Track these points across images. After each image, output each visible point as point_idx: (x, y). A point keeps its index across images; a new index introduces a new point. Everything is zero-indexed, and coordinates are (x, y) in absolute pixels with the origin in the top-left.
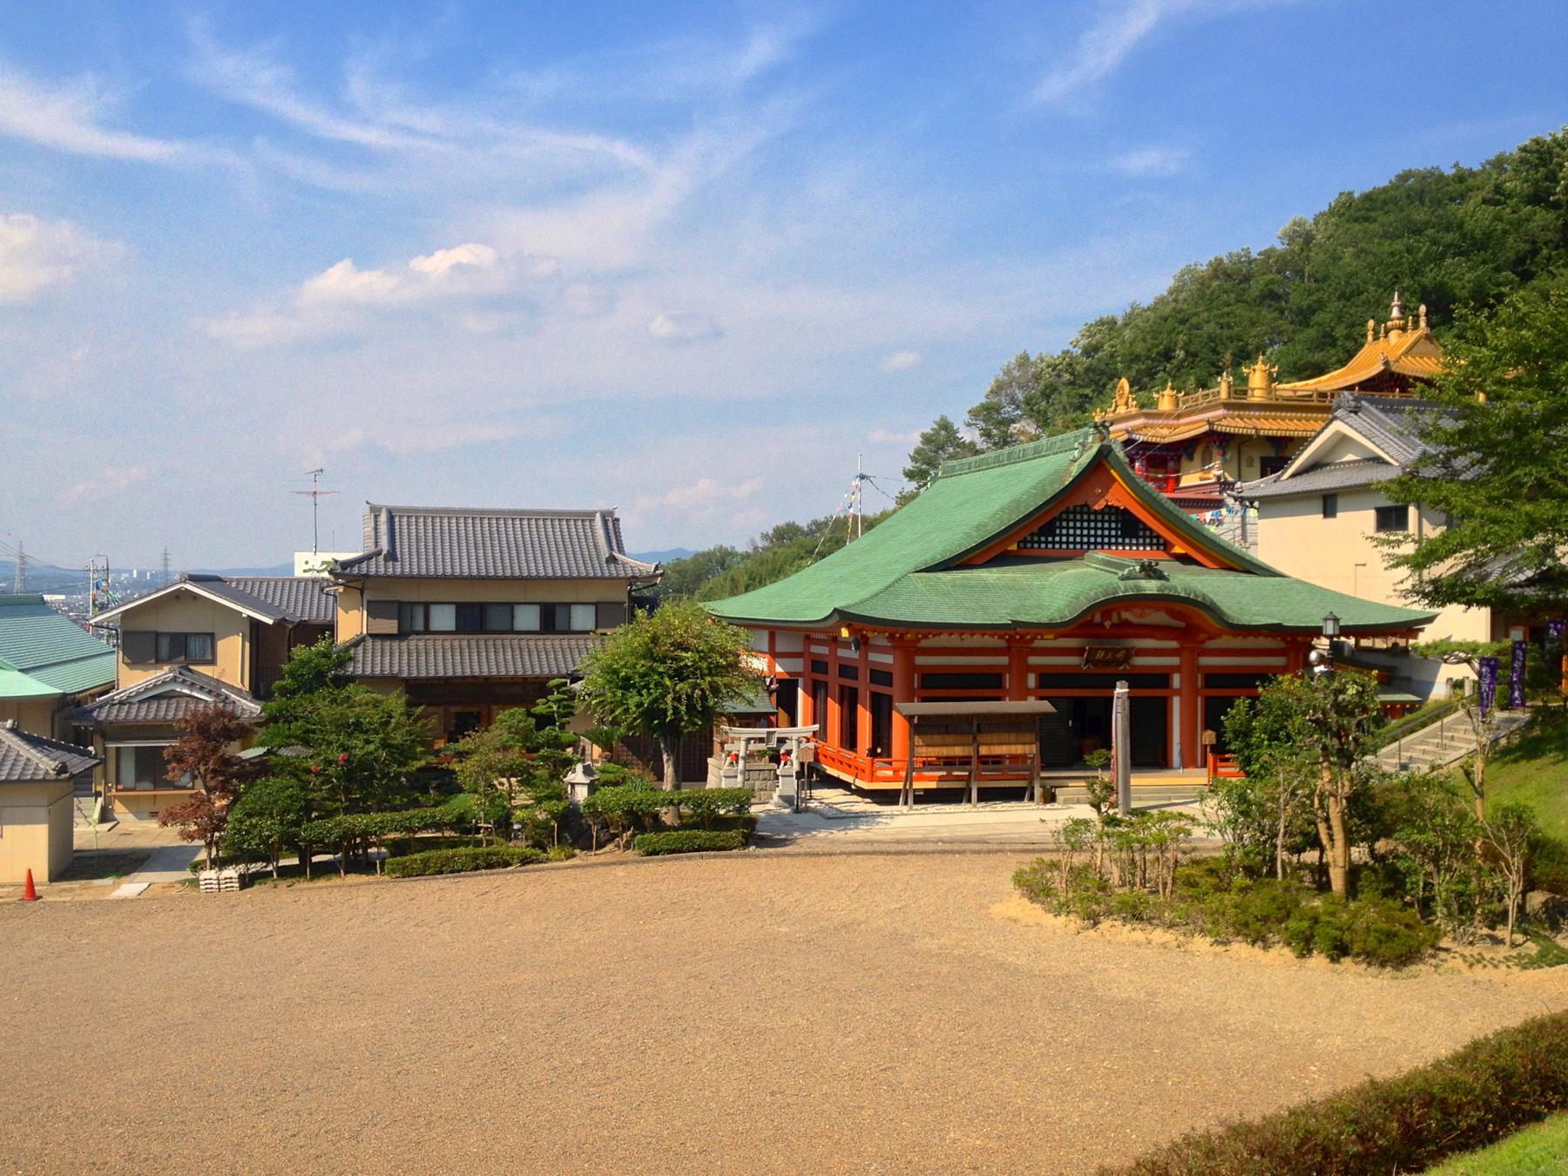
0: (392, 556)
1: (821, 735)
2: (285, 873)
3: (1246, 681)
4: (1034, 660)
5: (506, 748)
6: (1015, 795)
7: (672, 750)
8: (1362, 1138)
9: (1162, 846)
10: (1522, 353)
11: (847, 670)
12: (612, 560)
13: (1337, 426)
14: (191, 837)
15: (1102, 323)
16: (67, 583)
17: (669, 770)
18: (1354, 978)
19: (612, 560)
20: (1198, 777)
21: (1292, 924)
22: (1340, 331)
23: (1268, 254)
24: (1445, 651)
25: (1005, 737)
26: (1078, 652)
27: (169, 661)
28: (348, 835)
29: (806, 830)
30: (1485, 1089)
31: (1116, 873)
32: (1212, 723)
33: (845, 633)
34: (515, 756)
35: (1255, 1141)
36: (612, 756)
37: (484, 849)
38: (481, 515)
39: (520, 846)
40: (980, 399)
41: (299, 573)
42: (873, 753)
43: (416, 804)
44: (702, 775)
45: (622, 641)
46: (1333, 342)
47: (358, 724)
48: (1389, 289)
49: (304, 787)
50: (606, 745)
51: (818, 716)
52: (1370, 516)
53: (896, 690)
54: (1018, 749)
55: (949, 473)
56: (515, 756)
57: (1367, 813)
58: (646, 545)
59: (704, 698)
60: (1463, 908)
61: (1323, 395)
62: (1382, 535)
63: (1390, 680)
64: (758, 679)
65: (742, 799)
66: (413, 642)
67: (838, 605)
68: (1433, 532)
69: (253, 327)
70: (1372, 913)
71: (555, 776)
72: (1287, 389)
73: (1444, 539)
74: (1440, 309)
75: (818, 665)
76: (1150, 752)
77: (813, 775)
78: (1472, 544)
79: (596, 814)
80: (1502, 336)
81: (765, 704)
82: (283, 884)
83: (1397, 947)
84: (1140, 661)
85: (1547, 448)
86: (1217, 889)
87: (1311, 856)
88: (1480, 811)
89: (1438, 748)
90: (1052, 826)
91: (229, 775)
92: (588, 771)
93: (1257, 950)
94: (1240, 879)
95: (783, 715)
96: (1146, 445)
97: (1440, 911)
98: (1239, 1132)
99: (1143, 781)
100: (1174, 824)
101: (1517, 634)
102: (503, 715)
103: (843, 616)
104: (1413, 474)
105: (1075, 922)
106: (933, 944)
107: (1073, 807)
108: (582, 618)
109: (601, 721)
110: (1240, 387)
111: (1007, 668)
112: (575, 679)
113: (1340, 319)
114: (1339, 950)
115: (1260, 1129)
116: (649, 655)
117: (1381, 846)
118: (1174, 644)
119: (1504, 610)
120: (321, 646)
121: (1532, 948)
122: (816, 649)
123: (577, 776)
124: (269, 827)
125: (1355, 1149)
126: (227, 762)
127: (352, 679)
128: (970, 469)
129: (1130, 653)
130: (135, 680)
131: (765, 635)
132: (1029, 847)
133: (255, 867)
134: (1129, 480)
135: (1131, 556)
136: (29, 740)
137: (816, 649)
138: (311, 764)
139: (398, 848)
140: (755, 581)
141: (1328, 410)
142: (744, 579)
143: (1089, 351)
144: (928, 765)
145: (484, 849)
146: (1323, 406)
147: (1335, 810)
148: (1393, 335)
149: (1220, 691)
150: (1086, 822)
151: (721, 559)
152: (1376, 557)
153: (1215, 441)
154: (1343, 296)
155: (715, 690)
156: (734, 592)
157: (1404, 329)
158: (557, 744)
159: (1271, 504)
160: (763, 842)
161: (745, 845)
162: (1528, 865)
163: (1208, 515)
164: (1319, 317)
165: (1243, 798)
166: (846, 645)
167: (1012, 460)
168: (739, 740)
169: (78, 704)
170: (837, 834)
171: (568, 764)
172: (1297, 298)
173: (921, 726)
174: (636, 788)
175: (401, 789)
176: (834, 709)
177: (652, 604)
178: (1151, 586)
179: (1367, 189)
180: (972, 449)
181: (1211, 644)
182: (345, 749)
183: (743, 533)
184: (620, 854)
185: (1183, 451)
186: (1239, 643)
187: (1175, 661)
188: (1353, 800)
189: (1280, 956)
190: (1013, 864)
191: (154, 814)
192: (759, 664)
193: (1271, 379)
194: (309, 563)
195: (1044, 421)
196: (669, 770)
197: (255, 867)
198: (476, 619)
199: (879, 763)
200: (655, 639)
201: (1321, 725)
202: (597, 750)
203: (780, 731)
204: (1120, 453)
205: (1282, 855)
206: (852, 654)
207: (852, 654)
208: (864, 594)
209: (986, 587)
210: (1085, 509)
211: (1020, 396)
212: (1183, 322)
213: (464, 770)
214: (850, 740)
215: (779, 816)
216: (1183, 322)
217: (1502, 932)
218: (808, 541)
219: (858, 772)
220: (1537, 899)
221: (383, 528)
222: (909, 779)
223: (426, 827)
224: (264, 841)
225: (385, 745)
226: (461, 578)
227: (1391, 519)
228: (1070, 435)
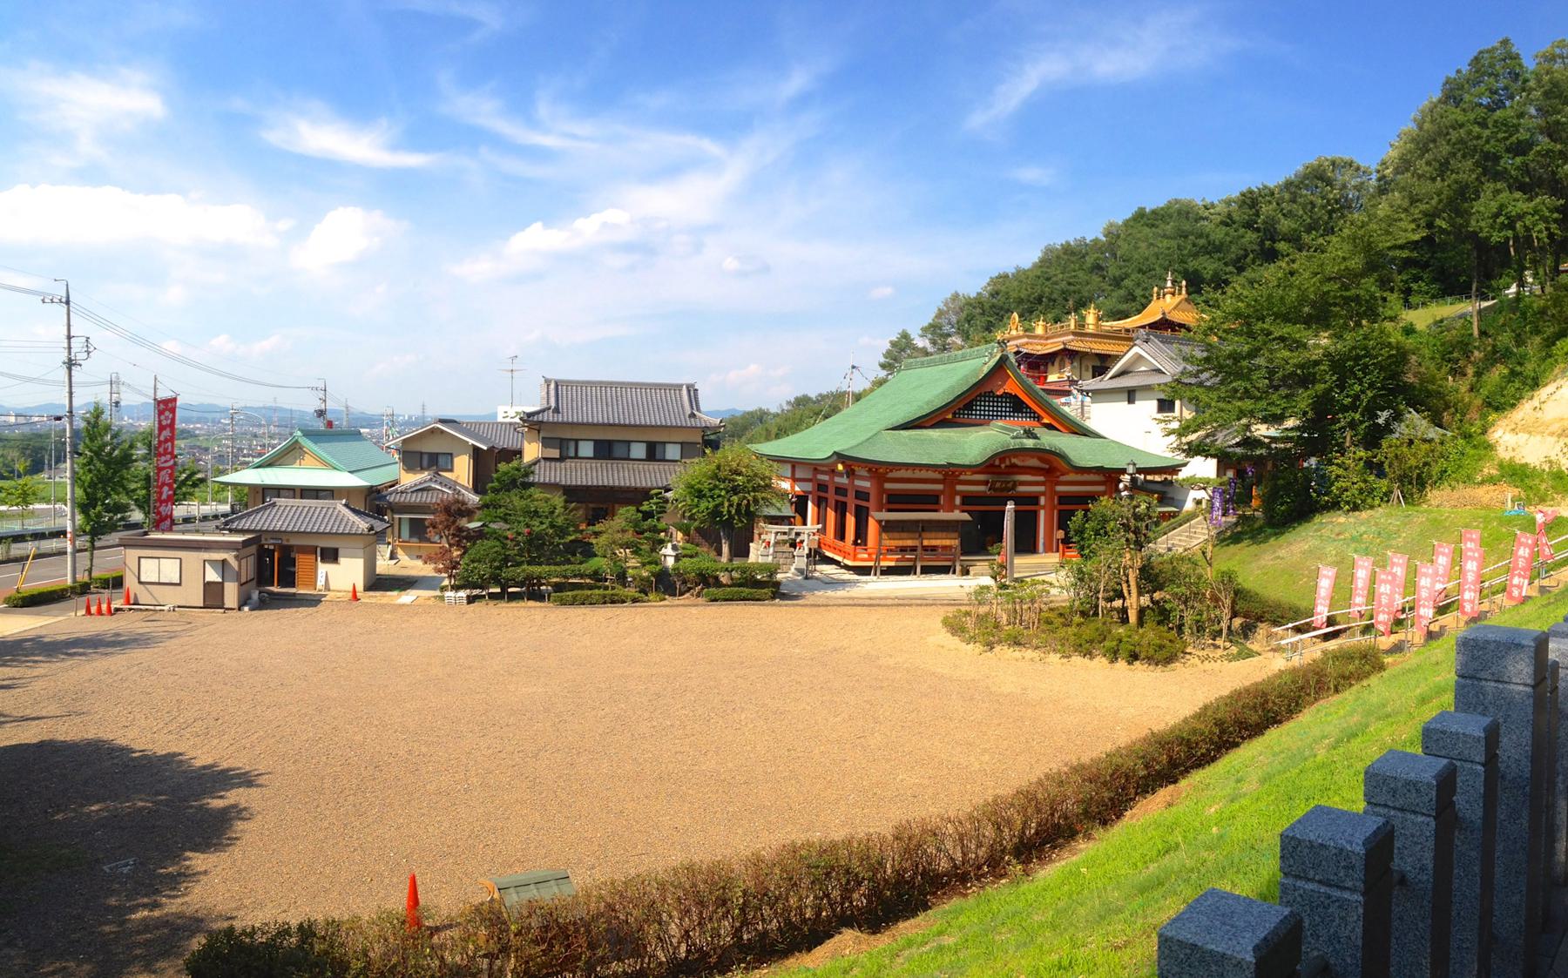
0: (557, 410)
1: (823, 531)
2: (493, 596)
3: (1083, 500)
4: (959, 488)
5: (624, 531)
6: (944, 570)
7: (729, 538)
8: (1147, 767)
9: (1033, 601)
10: (1238, 315)
11: (840, 490)
12: (693, 415)
13: (1136, 350)
14: (440, 571)
15: (1000, 277)
16: (372, 422)
17: (725, 549)
18: (1142, 674)
19: (693, 415)
20: (1054, 558)
21: (1107, 643)
22: (1139, 292)
23: (1096, 241)
24: (1193, 483)
25: (940, 535)
26: (986, 483)
27: (427, 469)
28: (529, 578)
29: (812, 590)
30: (1211, 732)
31: (1005, 617)
32: (1062, 525)
33: (840, 467)
34: (629, 536)
35: (1087, 775)
36: (689, 538)
37: (609, 592)
38: (611, 385)
39: (631, 591)
40: (928, 319)
41: (500, 419)
42: (855, 543)
43: (569, 562)
44: (747, 554)
45: (698, 469)
46: (1134, 299)
47: (536, 512)
48: (1166, 270)
49: (504, 546)
50: (686, 532)
51: (821, 519)
52: (1154, 404)
53: (871, 504)
54: (947, 542)
55: (909, 367)
56: (629, 536)
57: (1150, 578)
58: (715, 406)
59: (748, 505)
60: (1200, 628)
61: (1128, 331)
62: (1160, 416)
63: (1163, 500)
64: (783, 495)
65: (772, 570)
66: (568, 463)
67: (837, 449)
68: (1188, 415)
69: (478, 268)
70: (1151, 635)
71: (653, 550)
72: (1109, 325)
73: (1194, 419)
74: (1195, 284)
75: (822, 487)
76: (1026, 544)
77: (817, 556)
78: (1210, 422)
79: (679, 575)
80: (1229, 304)
81: (788, 511)
82: (492, 603)
83: (1164, 653)
84: (1021, 489)
85: (1250, 370)
86: (1065, 625)
87: (1118, 603)
88: (1209, 574)
89: (1188, 538)
90: (967, 590)
91: (463, 538)
92: (674, 548)
93: (1086, 660)
94: (1077, 619)
95: (798, 517)
96: (1028, 355)
97: (1187, 630)
98: (1078, 769)
99: (1021, 561)
100: (1040, 587)
101: (1230, 474)
102: (622, 510)
103: (839, 456)
104: (1178, 381)
105: (979, 648)
106: (891, 662)
107: (980, 578)
108: (673, 452)
109: (683, 516)
110: (1081, 324)
111: (942, 492)
112: (667, 490)
113: (1139, 285)
114: (1133, 657)
115: (1090, 767)
116: (715, 477)
117: (1157, 596)
118: (1041, 479)
119: (1224, 460)
120: (515, 464)
121: (1234, 650)
122: (821, 477)
123: (668, 550)
124: (484, 569)
125: (1142, 773)
126: (460, 529)
127: (532, 484)
128: (923, 365)
129: (1016, 484)
130: (409, 479)
131: (789, 467)
132: (953, 603)
133: (476, 592)
134: (1018, 376)
135: (1018, 424)
136: (354, 511)
137: (821, 477)
138: (508, 534)
139: (559, 588)
140: (781, 433)
141: (1130, 339)
142: (775, 430)
143: (995, 294)
144: (890, 551)
145: (609, 592)
146: (1127, 337)
147: (1133, 576)
148: (1168, 297)
149: (1068, 506)
150: (988, 588)
151: (760, 417)
152: (1157, 429)
153: (1068, 355)
154: (1140, 271)
155: (756, 501)
156: (768, 439)
157: (1173, 294)
158: (656, 530)
159: (1098, 395)
160: (784, 597)
161: (773, 598)
162: (1234, 603)
163: (1063, 400)
164: (1126, 282)
165: (1080, 571)
166: (840, 474)
167: (950, 361)
168: (771, 533)
169: (379, 492)
170: (830, 593)
171: (662, 542)
172: (1113, 271)
173: (887, 527)
174: (705, 560)
175: (560, 553)
176: (831, 515)
177: (715, 445)
178: (1029, 443)
179: (1154, 207)
180: (926, 353)
181: (1063, 478)
182: (528, 526)
183: (775, 400)
184: (693, 600)
185: (1050, 358)
186: (1079, 477)
187: (1042, 489)
188: (1142, 570)
189: (1100, 662)
190: (942, 612)
191: (419, 557)
192: (786, 485)
193: (1099, 319)
194: (508, 412)
195: (966, 337)
196: (725, 549)
197: (476, 592)
198: (606, 450)
199: (859, 549)
200: (718, 467)
201: (1126, 527)
202: (680, 535)
203: (798, 528)
204: (1013, 359)
205: (1102, 603)
206: (844, 480)
207: (844, 480)
208: (854, 443)
209: (931, 440)
210: (991, 394)
211: (954, 319)
212: (1048, 279)
213: (599, 543)
214: (841, 534)
215: (794, 581)
216: (1048, 279)
217: (1219, 642)
218: (816, 407)
219: (846, 555)
220: (1237, 622)
221: (552, 393)
222: (878, 560)
223: (575, 576)
224: (481, 577)
225: (552, 526)
226: (598, 425)
227: (1165, 406)
228: (983, 347)
